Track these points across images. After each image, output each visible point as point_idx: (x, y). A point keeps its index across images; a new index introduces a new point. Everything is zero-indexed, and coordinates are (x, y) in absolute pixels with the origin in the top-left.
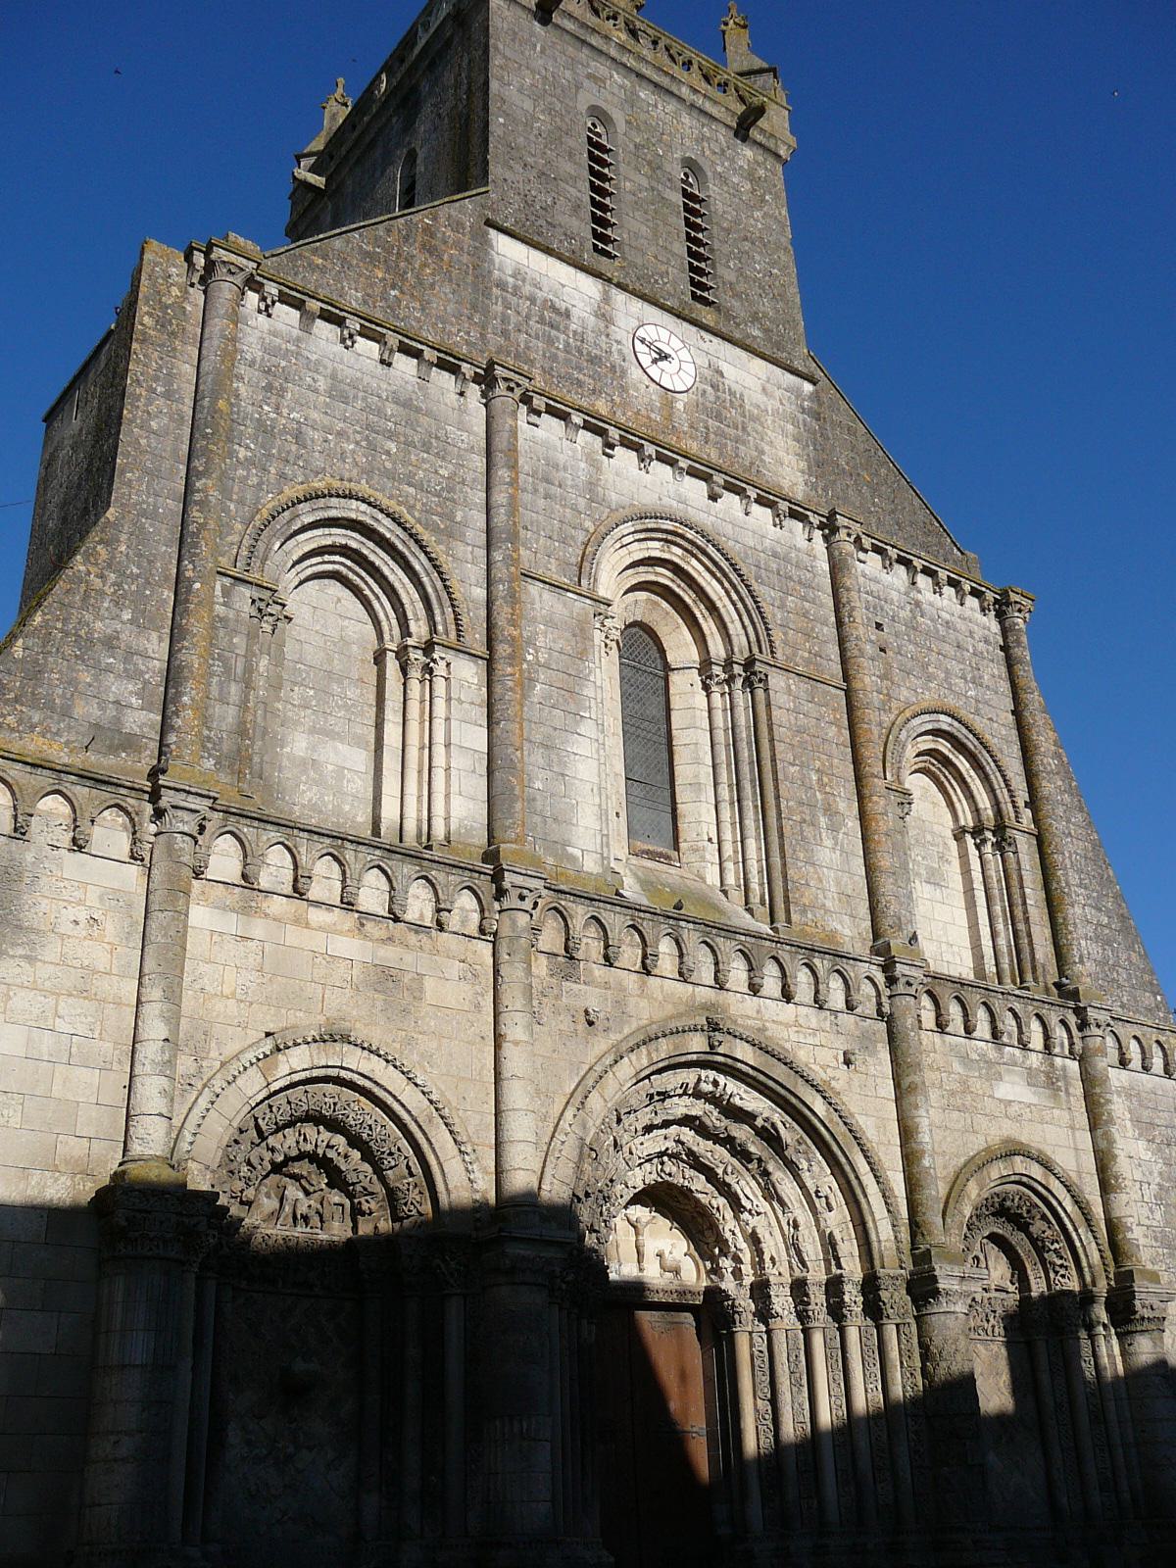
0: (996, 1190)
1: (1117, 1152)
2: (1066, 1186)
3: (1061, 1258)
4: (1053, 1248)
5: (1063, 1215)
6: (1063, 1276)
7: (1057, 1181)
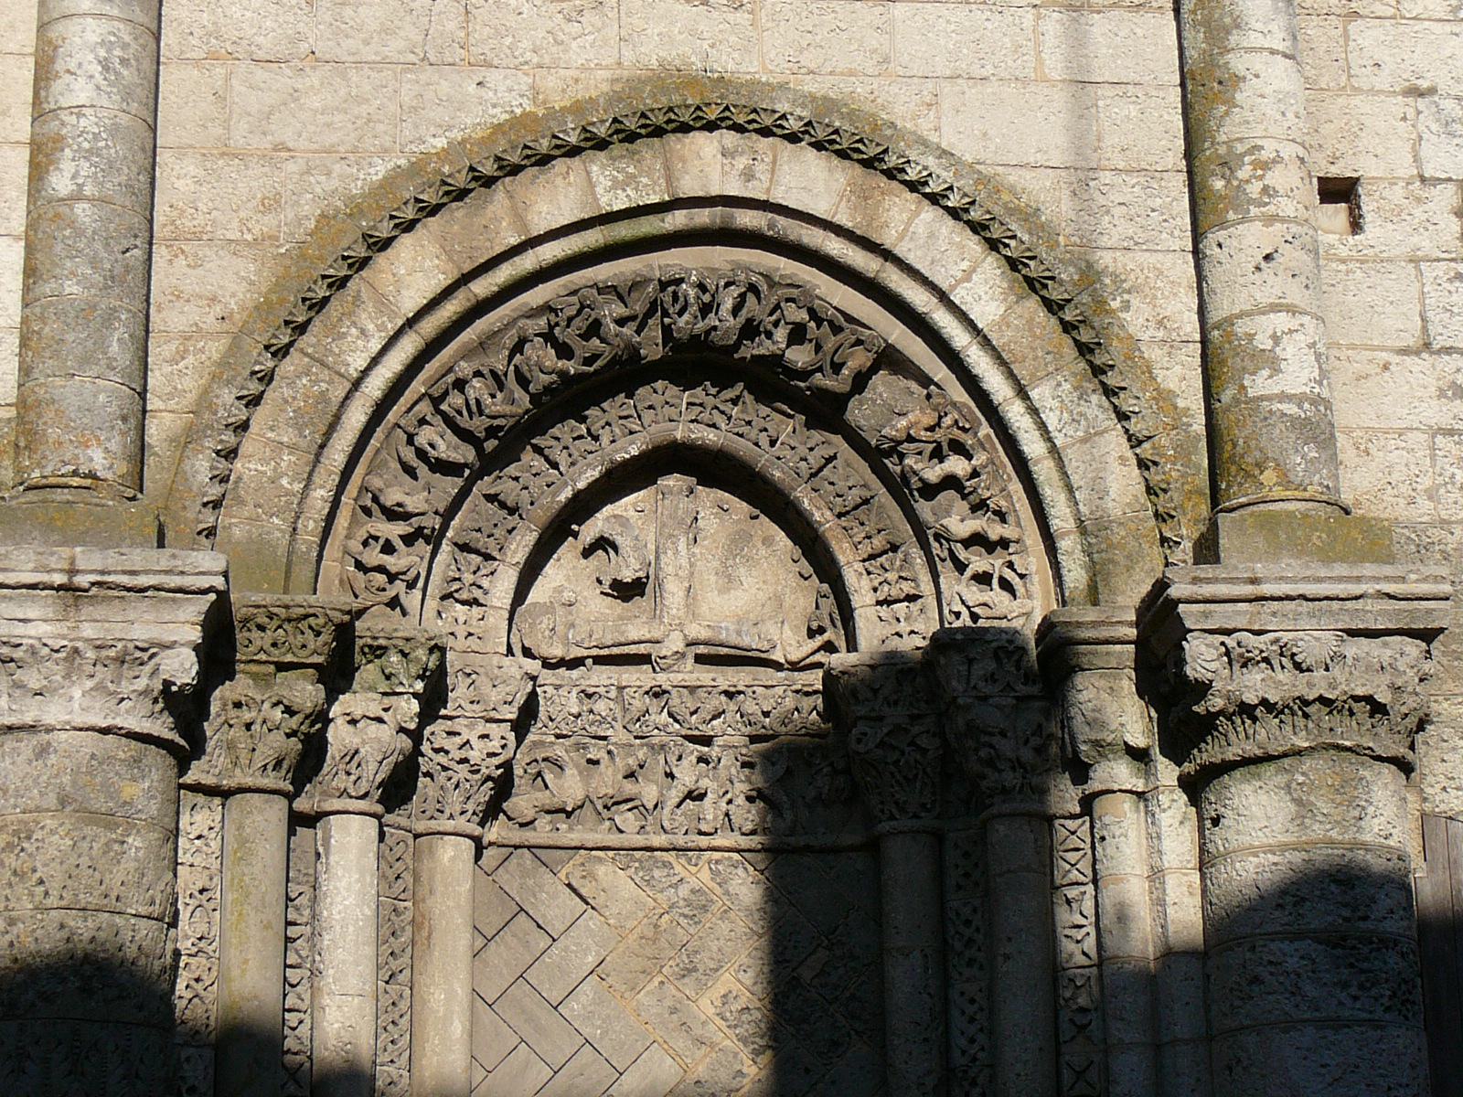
1: (1238, 63)
2: (977, 228)
3: (979, 507)
5: (959, 337)
6: (983, 579)
7: (929, 213)
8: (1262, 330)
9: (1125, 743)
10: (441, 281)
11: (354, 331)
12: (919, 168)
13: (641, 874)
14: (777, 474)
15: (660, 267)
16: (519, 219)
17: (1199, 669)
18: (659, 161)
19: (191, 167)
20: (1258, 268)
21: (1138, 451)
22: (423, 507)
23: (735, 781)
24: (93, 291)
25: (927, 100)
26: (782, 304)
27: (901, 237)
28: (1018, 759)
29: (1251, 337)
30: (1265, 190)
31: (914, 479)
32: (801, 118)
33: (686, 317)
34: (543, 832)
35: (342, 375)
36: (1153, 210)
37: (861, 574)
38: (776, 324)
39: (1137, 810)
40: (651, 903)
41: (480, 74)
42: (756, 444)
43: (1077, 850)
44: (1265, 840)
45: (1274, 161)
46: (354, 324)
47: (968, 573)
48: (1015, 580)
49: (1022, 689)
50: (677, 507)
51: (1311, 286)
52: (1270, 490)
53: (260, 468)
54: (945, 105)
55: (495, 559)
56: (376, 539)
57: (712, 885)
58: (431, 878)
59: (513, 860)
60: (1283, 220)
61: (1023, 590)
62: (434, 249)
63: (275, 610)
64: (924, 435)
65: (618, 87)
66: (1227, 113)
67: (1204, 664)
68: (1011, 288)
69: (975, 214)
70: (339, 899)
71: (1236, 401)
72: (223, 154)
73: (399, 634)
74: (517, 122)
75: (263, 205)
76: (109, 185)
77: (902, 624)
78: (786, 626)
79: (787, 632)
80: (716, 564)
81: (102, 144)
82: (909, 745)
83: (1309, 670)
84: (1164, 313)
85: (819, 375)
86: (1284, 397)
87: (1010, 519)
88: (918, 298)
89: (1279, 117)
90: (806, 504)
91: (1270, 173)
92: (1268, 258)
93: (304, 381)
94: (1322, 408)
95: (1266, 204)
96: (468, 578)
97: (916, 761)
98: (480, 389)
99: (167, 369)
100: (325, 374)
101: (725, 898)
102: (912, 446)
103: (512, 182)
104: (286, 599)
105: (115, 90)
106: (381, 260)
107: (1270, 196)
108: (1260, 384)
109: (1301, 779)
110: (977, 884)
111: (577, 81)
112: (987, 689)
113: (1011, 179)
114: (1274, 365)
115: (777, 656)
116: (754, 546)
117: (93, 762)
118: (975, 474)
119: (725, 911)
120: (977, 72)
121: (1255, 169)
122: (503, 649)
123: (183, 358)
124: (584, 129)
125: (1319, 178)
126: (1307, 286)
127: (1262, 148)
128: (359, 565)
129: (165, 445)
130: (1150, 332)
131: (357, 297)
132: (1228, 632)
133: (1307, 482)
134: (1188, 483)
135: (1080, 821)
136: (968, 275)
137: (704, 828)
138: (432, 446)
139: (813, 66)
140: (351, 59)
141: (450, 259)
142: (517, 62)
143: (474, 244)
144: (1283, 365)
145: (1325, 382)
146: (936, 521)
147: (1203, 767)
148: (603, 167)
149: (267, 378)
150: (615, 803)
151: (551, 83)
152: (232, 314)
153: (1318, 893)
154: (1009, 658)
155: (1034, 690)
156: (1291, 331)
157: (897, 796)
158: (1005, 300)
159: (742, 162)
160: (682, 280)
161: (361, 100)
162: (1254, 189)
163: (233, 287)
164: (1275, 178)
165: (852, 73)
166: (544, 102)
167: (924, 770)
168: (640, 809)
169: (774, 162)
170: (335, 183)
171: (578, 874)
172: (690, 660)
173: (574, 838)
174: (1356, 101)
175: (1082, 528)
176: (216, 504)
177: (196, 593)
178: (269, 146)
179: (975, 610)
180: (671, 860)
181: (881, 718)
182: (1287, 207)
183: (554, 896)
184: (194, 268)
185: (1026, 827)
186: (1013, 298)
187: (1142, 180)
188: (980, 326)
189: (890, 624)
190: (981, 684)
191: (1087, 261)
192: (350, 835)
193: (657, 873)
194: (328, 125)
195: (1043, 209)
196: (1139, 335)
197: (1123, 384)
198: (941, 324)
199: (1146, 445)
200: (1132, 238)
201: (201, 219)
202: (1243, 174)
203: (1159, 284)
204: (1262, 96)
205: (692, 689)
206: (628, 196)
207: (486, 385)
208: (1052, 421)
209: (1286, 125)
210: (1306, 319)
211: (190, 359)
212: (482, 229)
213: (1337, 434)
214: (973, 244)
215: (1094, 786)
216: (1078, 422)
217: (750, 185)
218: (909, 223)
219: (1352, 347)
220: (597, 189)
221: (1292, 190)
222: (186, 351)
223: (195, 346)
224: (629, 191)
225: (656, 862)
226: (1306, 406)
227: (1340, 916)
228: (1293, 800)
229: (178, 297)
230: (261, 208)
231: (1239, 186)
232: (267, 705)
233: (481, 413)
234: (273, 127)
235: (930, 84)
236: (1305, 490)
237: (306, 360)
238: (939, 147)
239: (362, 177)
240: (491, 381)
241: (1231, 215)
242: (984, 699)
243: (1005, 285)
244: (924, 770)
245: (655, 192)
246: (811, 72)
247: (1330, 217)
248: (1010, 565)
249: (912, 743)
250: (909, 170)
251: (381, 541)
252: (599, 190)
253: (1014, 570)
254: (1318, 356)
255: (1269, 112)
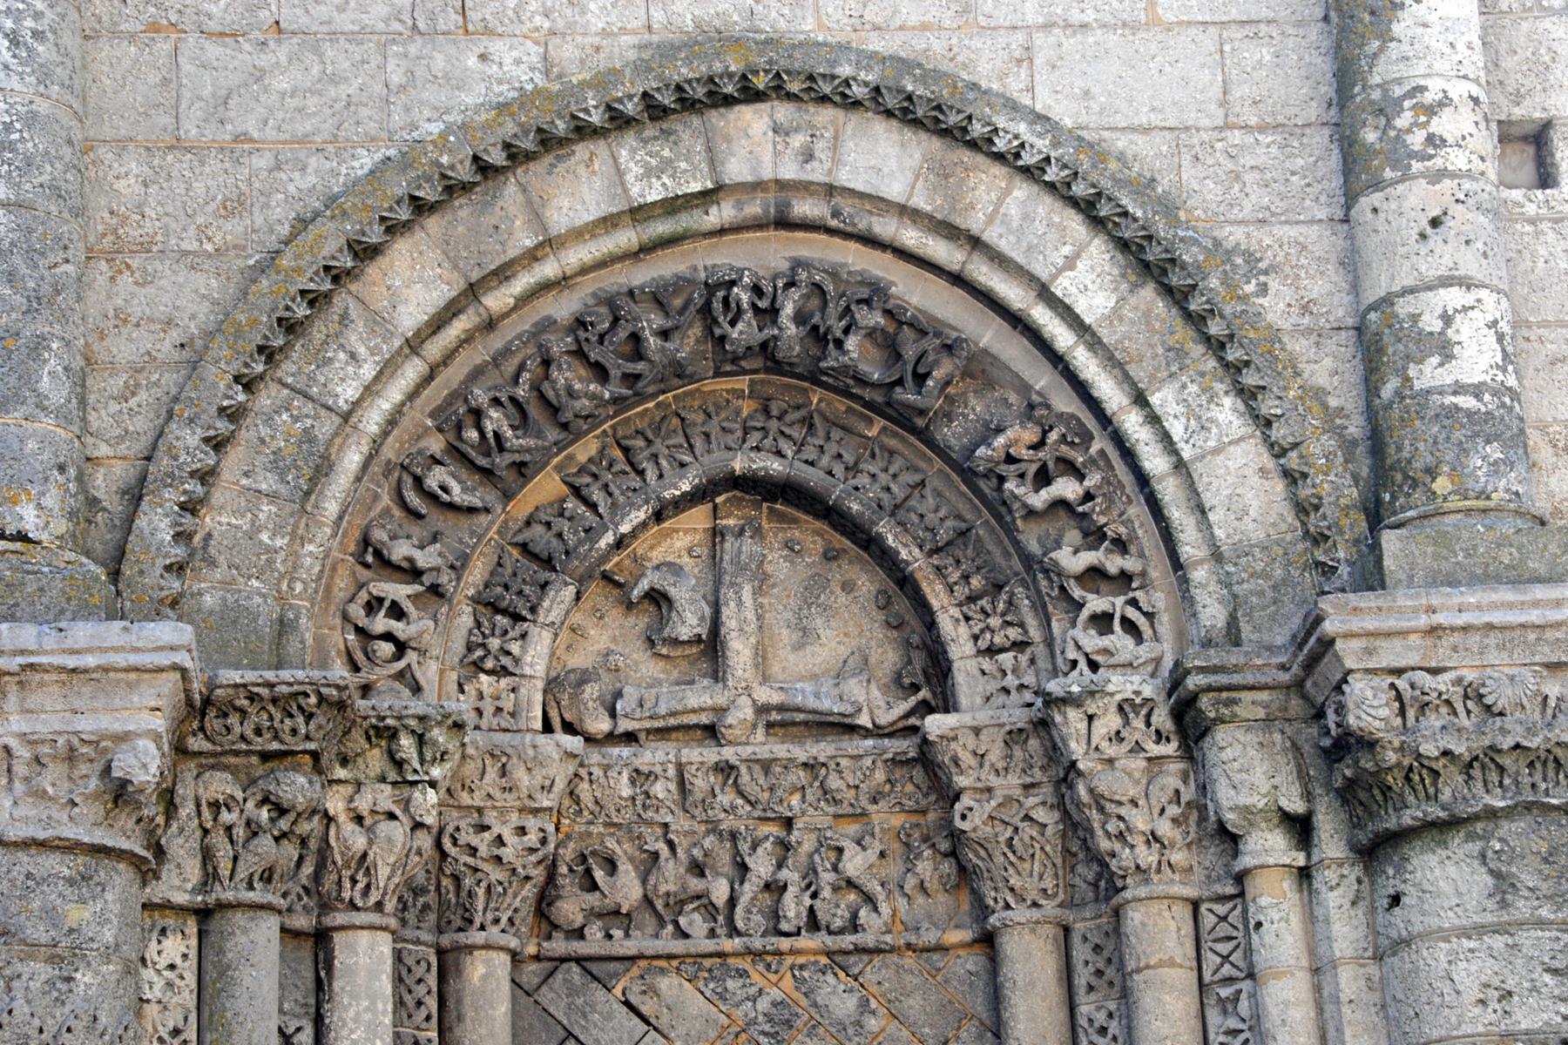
0: (642, 275)
3: (1094, 536)
4: (1039, 500)
5: (1063, 337)
6: (1102, 622)
7: (1022, 191)
8: (1429, 310)
9: (1280, 809)
10: (441, 294)
11: (342, 356)
12: (1009, 136)
13: (712, 985)
14: (855, 507)
15: (705, 268)
16: (536, 217)
17: (1364, 716)
18: (701, 141)
19: (133, 165)
20: (1423, 236)
21: (1282, 461)
22: (435, 561)
23: (820, 869)
24: (14, 315)
25: (1017, 54)
26: (853, 307)
27: (990, 219)
28: (1152, 833)
29: (1415, 318)
30: (1430, 139)
31: (1016, 506)
32: (866, 84)
33: (740, 326)
34: (594, 942)
35: (329, 409)
36: (1293, 173)
37: (957, 620)
38: (846, 331)
39: (1301, 891)
40: (724, 1020)
41: (485, 44)
42: (830, 473)
43: (1230, 938)
44: (1457, 922)
45: (1441, 104)
46: (342, 346)
47: (1085, 614)
48: (1141, 621)
49: (1155, 749)
50: (740, 552)
51: (1490, 253)
52: (1445, 499)
53: (234, 521)
54: (1039, 61)
55: (525, 619)
56: (380, 600)
57: (796, 995)
58: (459, 1002)
59: (559, 976)
60: (1452, 175)
61: (1150, 632)
62: (434, 255)
63: (256, 690)
64: (1025, 453)
65: (646, 55)
66: (1382, 49)
67: (1373, 712)
68: (1123, 275)
69: (1079, 189)
70: (345, 1033)
71: (1399, 394)
72: (172, 148)
73: (410, 712)
74: (526, 99)
75: (225, 208)
76: (28, 186)
77: (1010, 677)
78: (873, 686)
79: (876, 693)
80: (788, 615)
81: (16, 136)
82: (1023, 820)
83: (1501, 714)
84: (1308, 296)
85: (898, 390)
86: (1459, 389)
87: (1133, 549)
88: (1013, 293)
89: (1448, 50)
90: (890, 540)
91: (1435, 119)
92: (1435, 223)
93: (284, 417)
94: (1507, 400)
95: (1431, 157)
96: (494, 643)
97: (1032, 838)
98: (498, 420)
99: (114, 407)
100: (309, 408)
101: (813, 1011)
102: (1012, 467)
103: (526, 172)
104: (270, 675)
105: (28, 70)
106: (372, 270)
107: (1435, 147)
108: (1429, 374)
109: (1498, 847)
110: (1111, 984)
111: (598, 49)
112: (1111, 750)
113: (1120, 144)
114: (1446, 351)
115: (864, 720)
116: (832, 592)
117: (30, 883)
118: (1088, 497)
119: (814, 1027)
120: (1076, 17)
121: (1417, 115)
122: (538, 725)
123: (134, 394)
124: (609, 108)
125: (1500, 122)
126: (1485, 255)
127: (1426, 88)
128: (360, 631)
129: (116, 498)
130: (1294, 319)
131: (344, 318)
132: (1399, 672)
133: (1490, 488)
134: (1345, 496)
135: (1230, 905)
136: (1070, 263)
137: (784, 926)
138: (445, 489)
139: (879, 20)
140: (325, 29)
141: (455, 267)
142: (525, 29)
143: (483, 248)
144: (1457, 349)
145: (1510, 368)
146: (1045, 554)
147: (1377, 835)
148: (633, 151)
149: (234, 415)
150: (678, 904)
151: (567, 53)
152: (192, 339)
153: (1526, 985)
154: (1137, 714)
155: (1170, 749)
156: (1465, 309)
157: (1012, 881)
158: (1116, 289)
159: (798, 140)
160: (733, 283)
161: (335, 80)
162: (1416, 140)
163: (193, 308)
164: (1442, 125)
165: (925, 27)
166: (560, 76)
167: (1042, 848)
168: (710, 910)
169: (836, 138)
170: (312, 179)
171: (637, 987)
172: (760, 731)
173: (630, 947)
174: (1547, 24)
175: (1217, 556)
176: (177, 569)
177: (150, 671)
178: (228, 137)
179: (1095, 657)
180: (748, 967)
181: (989, 790)
182: (1457, 160)
183: (608, 1017)
184: (142, 285)
185: (1166, 914)
186: (1124, 286)
187: (1279, 138)
188: (1088, 321)
189: (994, 677)
190: (1104, 745)
191: (1215, 239)
192: (357, 955)
193: (730, 984)
194: (300, 110)
195: (1159, 178)
196: (1281, 324)
197: (1261, 383)
198: (1041, 321)
199: (1293, 454)
200: (1268, 208)
201: (149, 226)
202: (1402, 122)
203: (1303, 261)
204: (1425, 25)
205: (766, 766)
206: (664, 185)
207: (506, 416)
208: (1177, 429)
209: (1456, 58)
210: (1483, 294)
211: (143, 396)
212: (492, 230)
213: (1528, 431)
214: (1075, 224)
215: (1246, 861)
216: (1209, 430)
217: (808, 167)
218: (1000, 202)
219: (1545, 324)
220: (628, 177)
221: (1464, 138)
222: (137, 385)
223: (147, 378)
224: (665, 179)
225: (729, 969)
226: (1487, 397)
227: (1557, 1013)
228: (1491, 872)
229: (125, 321)
230: (222, 212)
231: (1397, 137)
232: (250, 805)
233: (501, 448)
234: (232, 114)
235: (1020, 37)
236: (1488, 498)
237: (286, 391)
238: (1033, 111)
239: (344, 171)
240: (511, 409)
241: (1388, 174)
242: (1110, 761)
243: (1116, 272)
244: (1042, 848)
245: (695, 179)
246: (876, 28)
247: (1514, 170)
248: (1134, 603)
249: (1027, 817)
250: (997, 140)
251: (387, 604)
252: (630, 178)
253: (1139, 609)
254: (1500, 338)
255: (1434, 44)
